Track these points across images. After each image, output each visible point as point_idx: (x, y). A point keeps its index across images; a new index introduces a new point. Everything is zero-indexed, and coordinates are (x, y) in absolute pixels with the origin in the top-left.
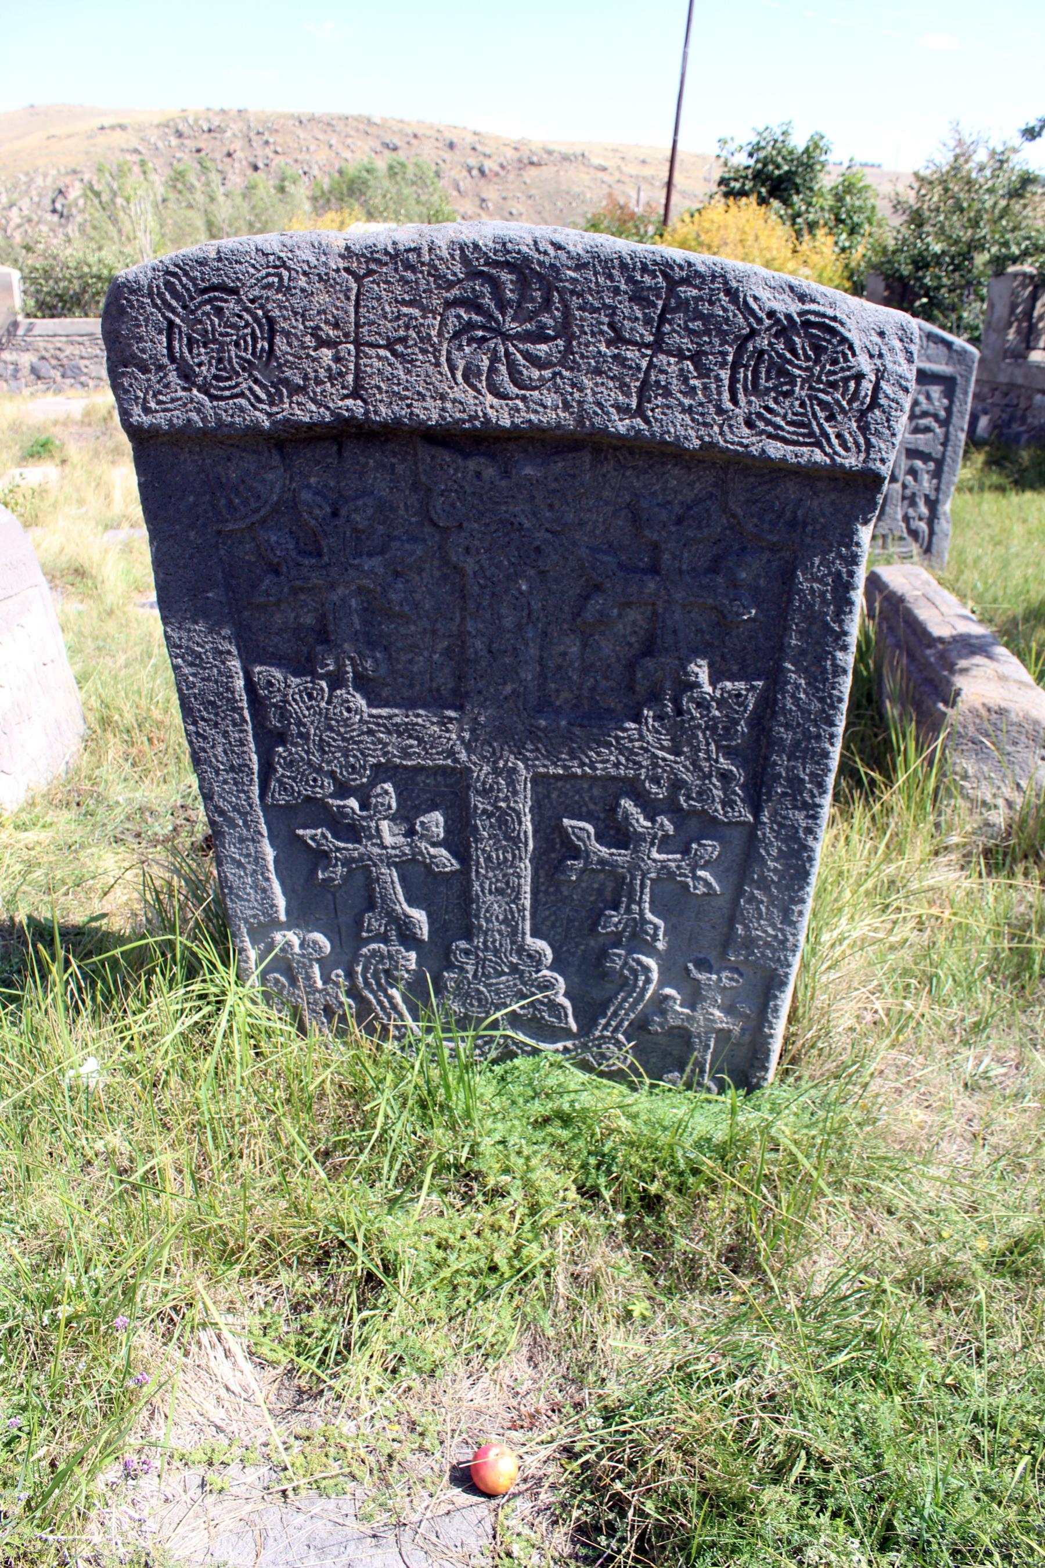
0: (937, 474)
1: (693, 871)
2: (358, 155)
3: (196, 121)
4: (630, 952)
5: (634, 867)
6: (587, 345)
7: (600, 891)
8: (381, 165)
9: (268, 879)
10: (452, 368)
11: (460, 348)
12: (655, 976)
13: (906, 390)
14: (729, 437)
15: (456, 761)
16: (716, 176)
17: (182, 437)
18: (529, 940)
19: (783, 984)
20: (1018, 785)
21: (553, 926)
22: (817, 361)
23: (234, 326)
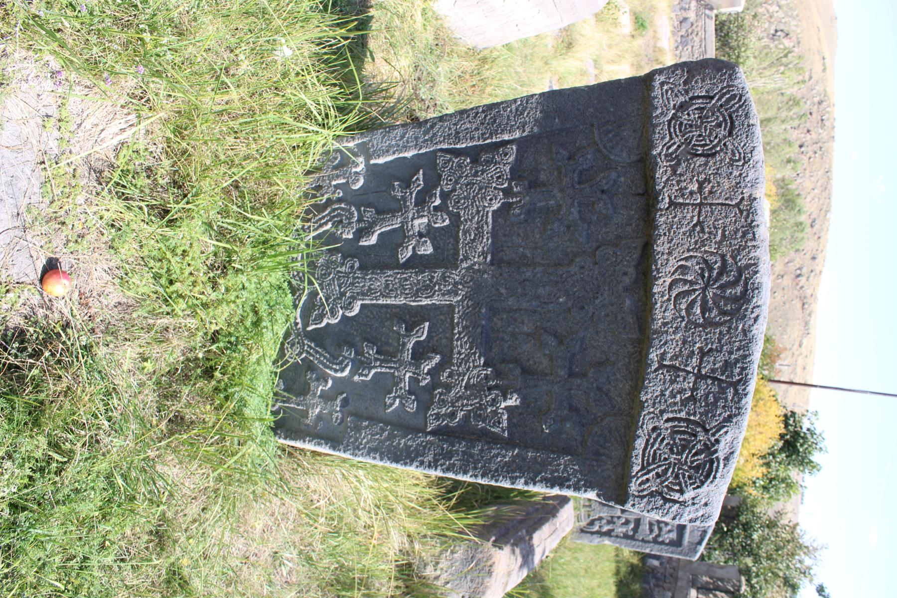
0: (626, 536)
1: (399, 397)
2: (808, 205)
3: (828, 112)
4: (352, 360)
5: (401, 363)
6: (700, 336)
7: (387, 343)
8: (803, 218)
9: (394, 153)
10: (686, 259)
11: (698, 263)
12: (339, 375)
13: (674, 519)
14: (647, 417)
15: (462, 261)
16: (796, 410)
17: (647, 104)
18: (359, 303)
19: (334, 448)
20: (448, 583)
21: (367, 316)
22: (690, 467)
23: (711, 134)
